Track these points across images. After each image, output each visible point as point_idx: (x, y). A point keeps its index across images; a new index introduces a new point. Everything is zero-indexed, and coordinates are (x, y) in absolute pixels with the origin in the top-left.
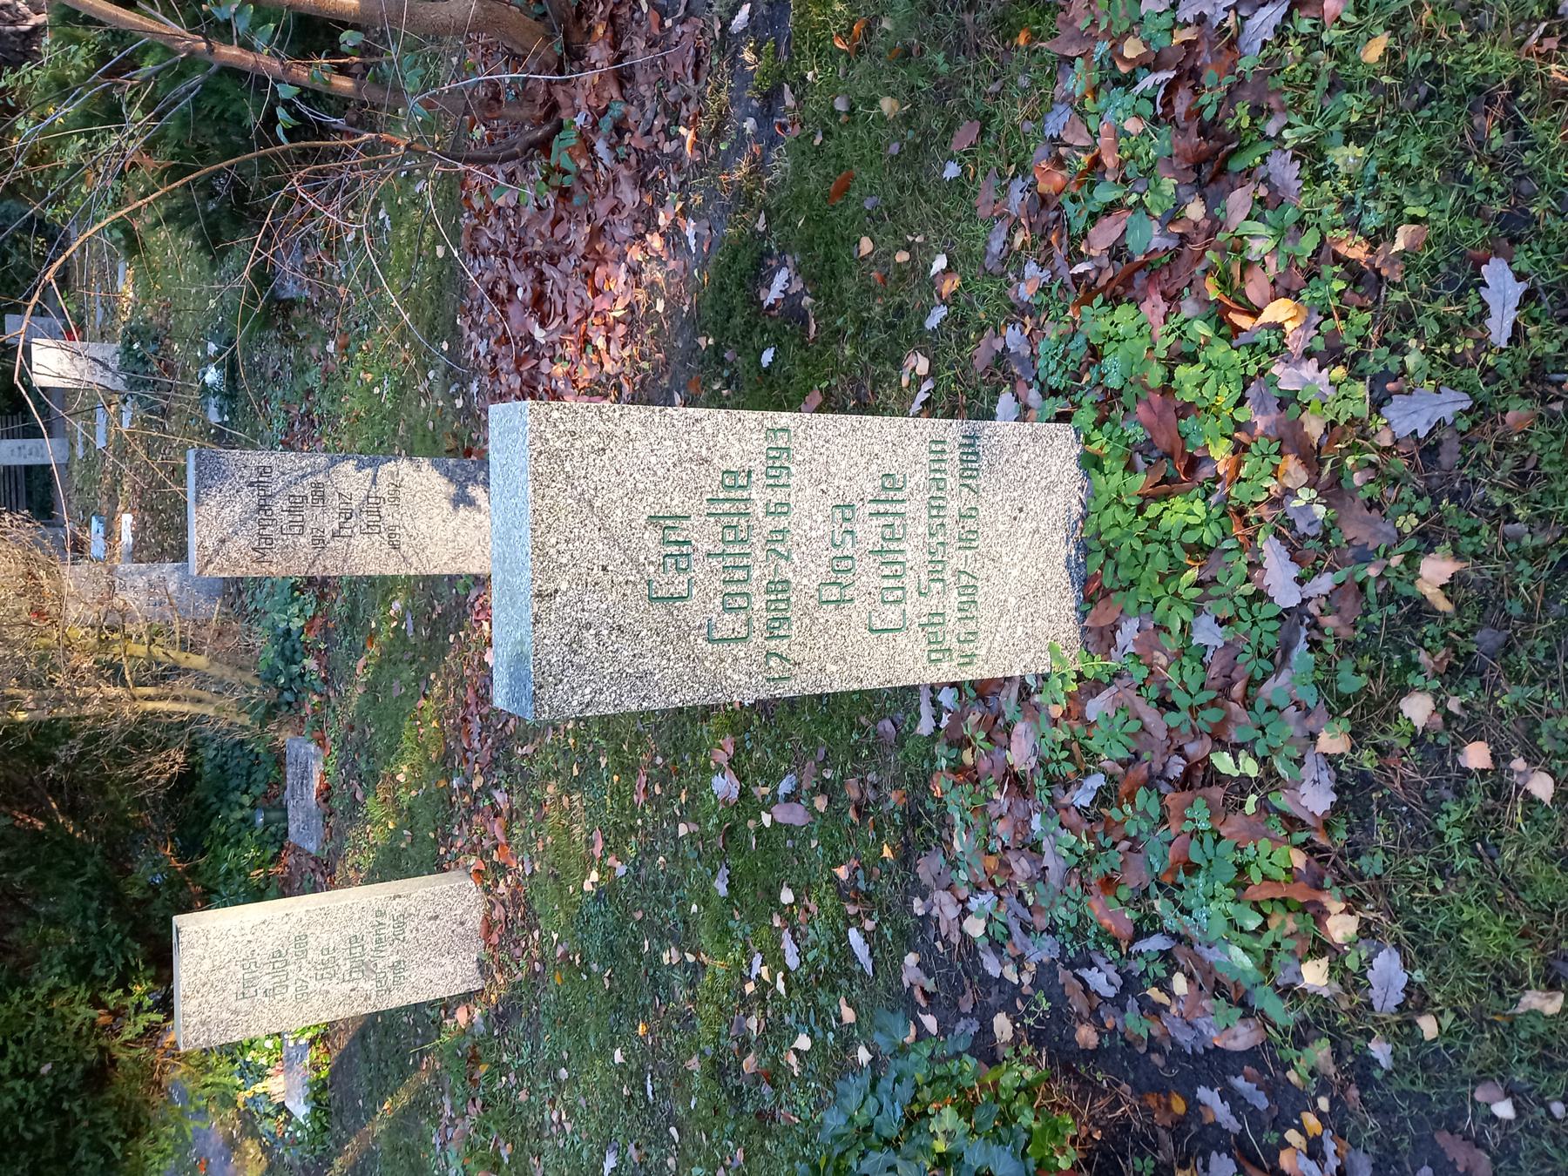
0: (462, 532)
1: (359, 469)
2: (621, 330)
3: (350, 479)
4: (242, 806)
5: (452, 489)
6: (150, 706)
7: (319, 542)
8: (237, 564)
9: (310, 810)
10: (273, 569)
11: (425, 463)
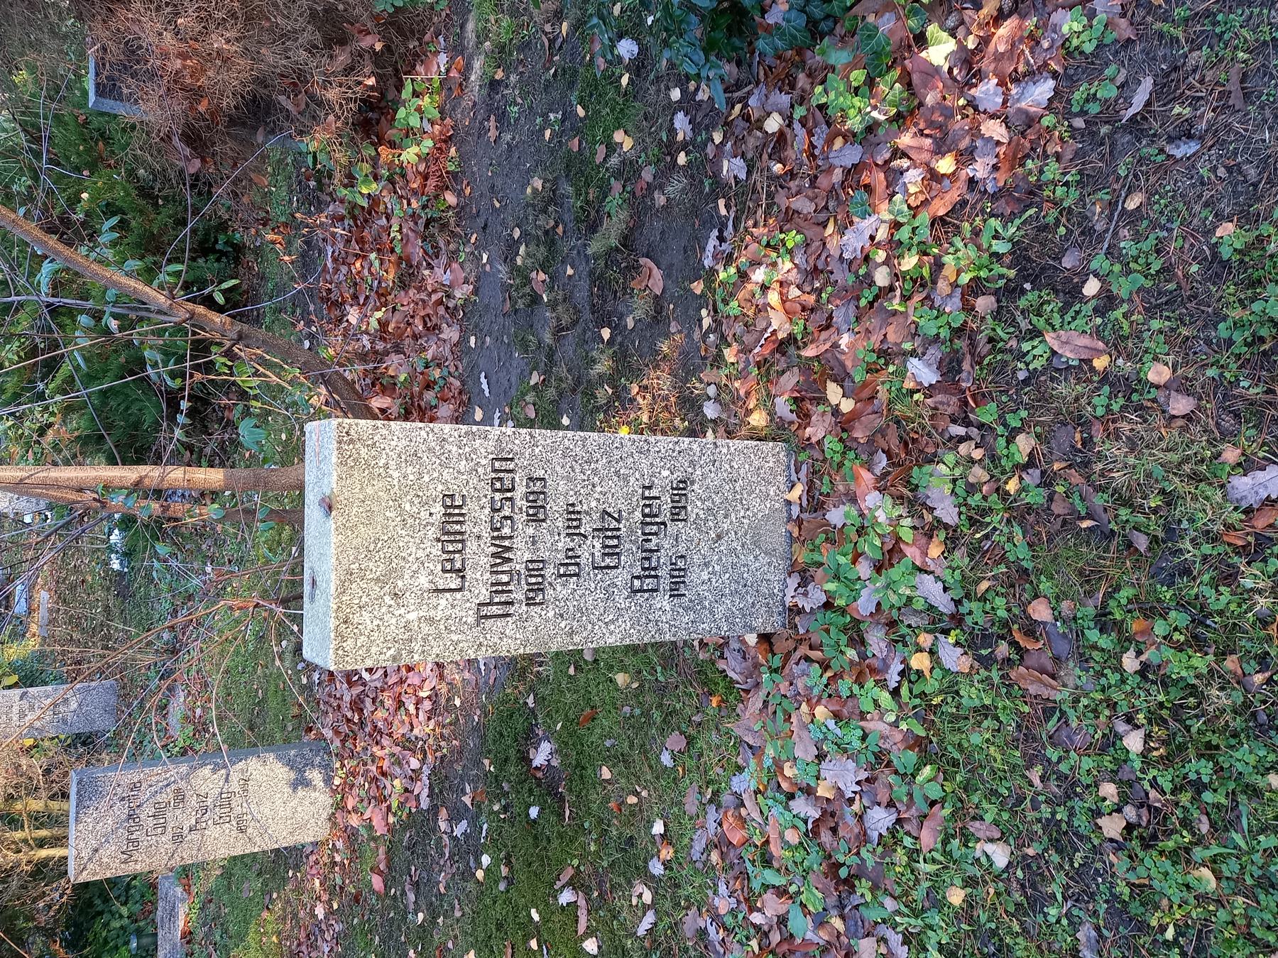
0: (299, 809)
1: (214, 771)
2: (427, 705)
3: (207, 780)
4: (121, 917)
5: (293, 775)
6: (44, 853)
7: (178, 838)
8: (108, 867)
9: (175, 944)
10: (138, 867)
11: (271, 757)
